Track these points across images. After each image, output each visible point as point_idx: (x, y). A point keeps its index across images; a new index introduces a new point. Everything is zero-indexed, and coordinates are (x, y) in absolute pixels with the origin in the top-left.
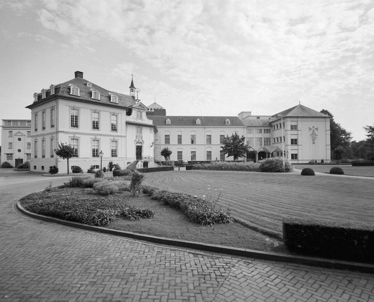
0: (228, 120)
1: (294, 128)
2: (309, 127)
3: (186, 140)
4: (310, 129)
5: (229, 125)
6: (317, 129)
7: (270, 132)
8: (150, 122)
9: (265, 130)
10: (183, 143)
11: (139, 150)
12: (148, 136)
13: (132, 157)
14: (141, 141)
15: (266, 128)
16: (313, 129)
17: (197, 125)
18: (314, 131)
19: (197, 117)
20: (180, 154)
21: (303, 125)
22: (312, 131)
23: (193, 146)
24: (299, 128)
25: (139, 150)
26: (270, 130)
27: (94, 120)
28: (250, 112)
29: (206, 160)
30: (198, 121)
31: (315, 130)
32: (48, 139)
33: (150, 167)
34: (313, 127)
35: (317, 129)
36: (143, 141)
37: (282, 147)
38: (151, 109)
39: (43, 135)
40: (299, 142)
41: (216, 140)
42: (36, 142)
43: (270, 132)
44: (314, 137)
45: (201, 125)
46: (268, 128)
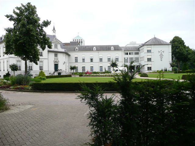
0: (112, 47)
1: (149, 51)
2: (158, 50)
3: (88, 60)
4: (159, 52)
5: (95, 51)
6: (163, 52)
7: (138, 54)
8: (63, 50)
9: (135, 53)
10: (85, 62)
11: (56, 66)
12: (62, 58)
13: (52, 69)
14: (57, 61)
15: (136, 52)
16: (161, 52)
17: (112, 50)
18: (161, 53)
19: (94, 46)
20: (84, 68)
21: (155, 49)
22: (160, 53)
23: (92, 63)
24: (152, 51)
25: (56, 66)
26: (138, 53)
27: (40, 65)
28: (136, 42)
29: (99, 71)
30: (112, 48)
31: (162, 52)
32: (5, 61)
33: (63, 75)
34: (161, 51)
35: (163, 52)
36: (58, 61)
37: (143, 63)
38: (76, 40)
39: (3, 59)
40: (152, 60)
41: (105, 59)
42: (4, 62)
43: (138, 54)
44: (161, 56)
45: (96, 51)
46: (137, 52)
